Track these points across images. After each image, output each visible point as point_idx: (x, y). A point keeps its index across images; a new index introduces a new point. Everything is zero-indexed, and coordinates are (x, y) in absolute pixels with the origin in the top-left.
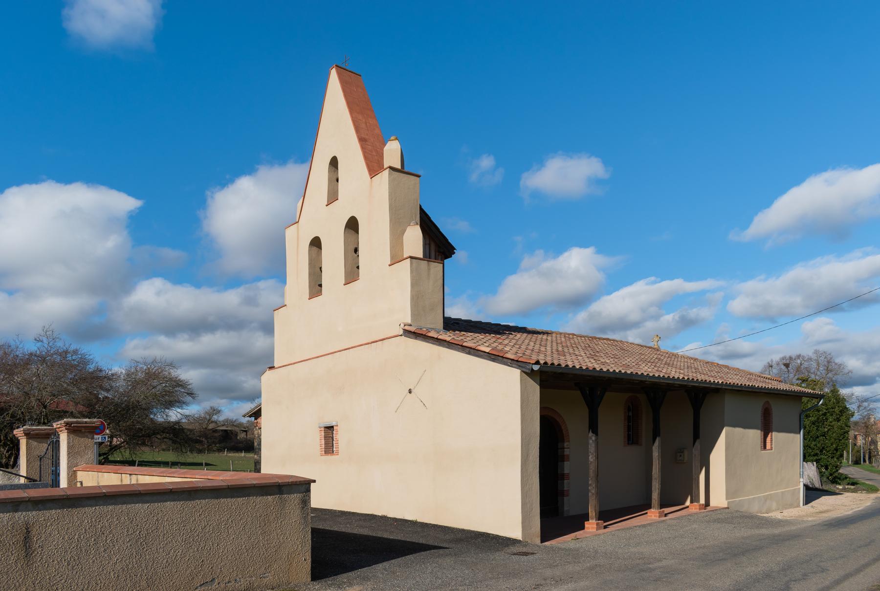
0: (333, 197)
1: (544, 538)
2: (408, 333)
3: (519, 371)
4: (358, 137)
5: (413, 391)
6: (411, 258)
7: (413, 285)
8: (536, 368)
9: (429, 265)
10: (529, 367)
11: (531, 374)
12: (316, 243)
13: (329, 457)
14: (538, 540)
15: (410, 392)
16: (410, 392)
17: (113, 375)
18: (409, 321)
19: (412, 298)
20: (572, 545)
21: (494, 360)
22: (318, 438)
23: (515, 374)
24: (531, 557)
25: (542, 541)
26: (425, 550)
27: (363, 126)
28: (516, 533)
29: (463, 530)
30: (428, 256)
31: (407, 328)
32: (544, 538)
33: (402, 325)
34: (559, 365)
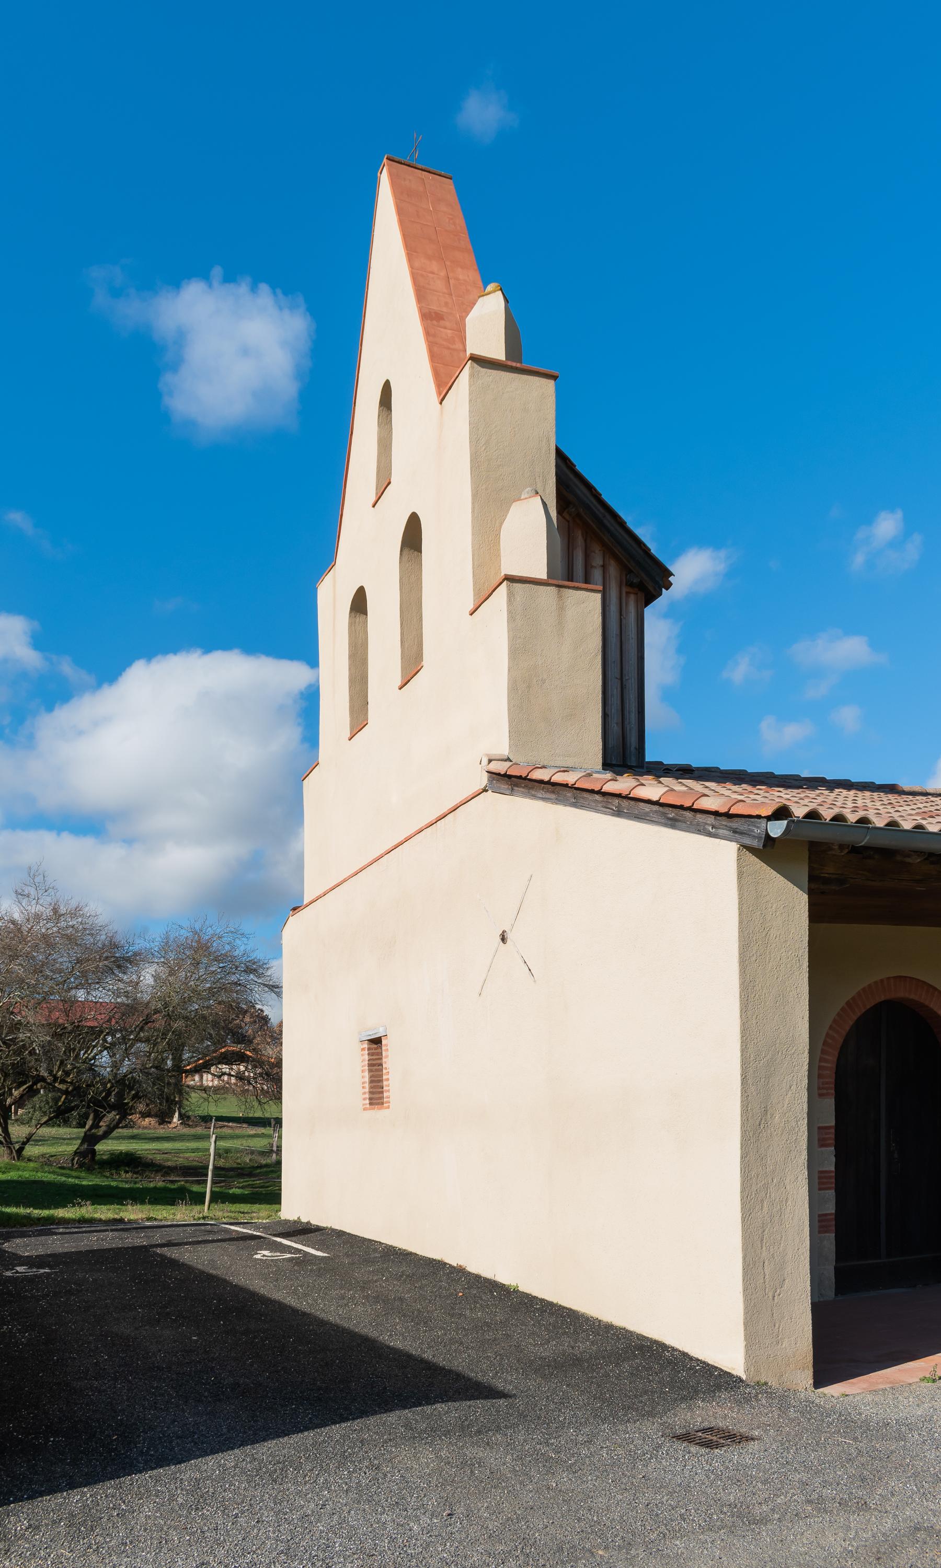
0: (384, 484)
1: (830, 1364)
2: (509, 781)
3: (732, 847)
4: (420, 310)
5: (510, 936)
6: (510, 579)
7: (515, 652)
8: (777, 829)
9: (560, 597)
10: (758, 829)
11: (768, 851)
12: (359, 604)
13: (379, 1114)
14: (805, 1378)
15: (503, 939)
16: (503, 939)
17: (135, 954)
18: (505, 751)
19: (513, 688)
20: (908, 1408)
21: (673, 823)
22: (359, 1069)
23: (722, 855)
24: (732, 1455)
25: (820, 1380)
26: (445, 1396)
27: (439, 285)
28: (730, 1357)
29: (609, 1327)
30: (567, 571)
31: (501, 767)
32: (830, 1364)
33: (485, 761)
34: (864, 821)
